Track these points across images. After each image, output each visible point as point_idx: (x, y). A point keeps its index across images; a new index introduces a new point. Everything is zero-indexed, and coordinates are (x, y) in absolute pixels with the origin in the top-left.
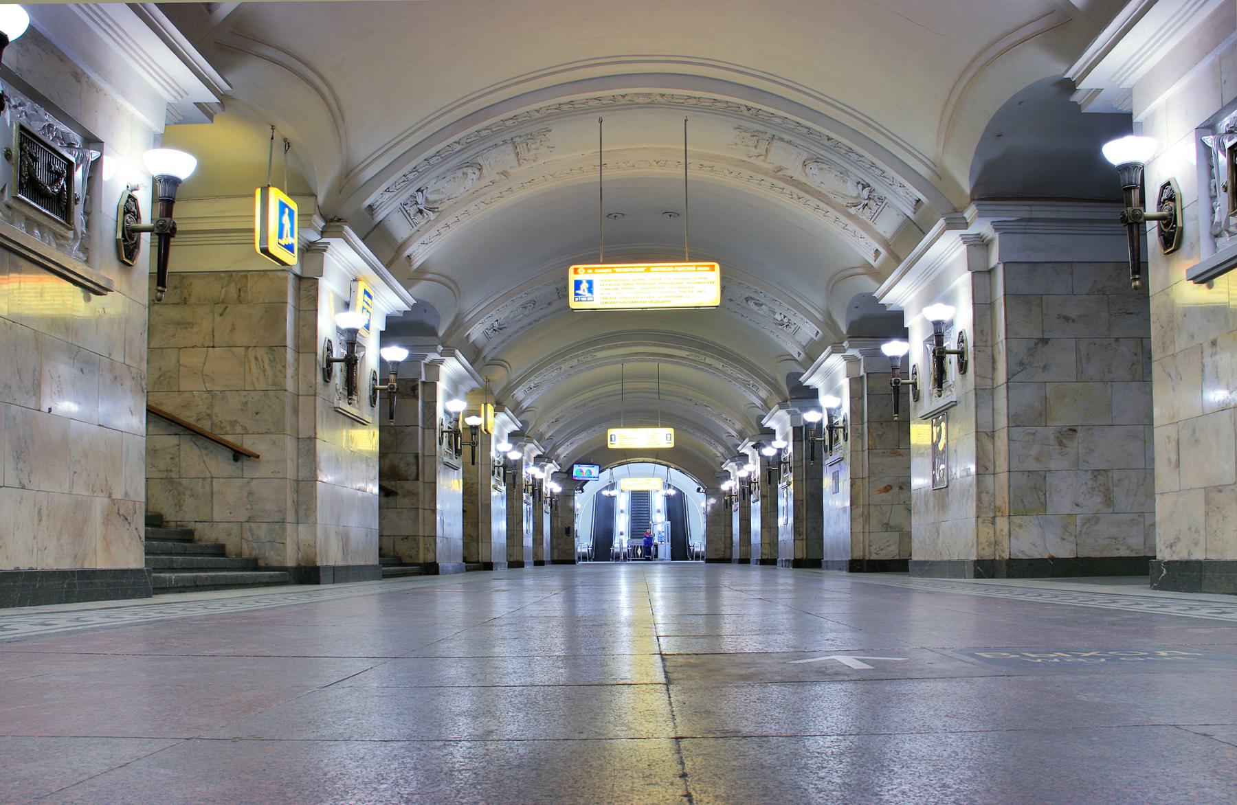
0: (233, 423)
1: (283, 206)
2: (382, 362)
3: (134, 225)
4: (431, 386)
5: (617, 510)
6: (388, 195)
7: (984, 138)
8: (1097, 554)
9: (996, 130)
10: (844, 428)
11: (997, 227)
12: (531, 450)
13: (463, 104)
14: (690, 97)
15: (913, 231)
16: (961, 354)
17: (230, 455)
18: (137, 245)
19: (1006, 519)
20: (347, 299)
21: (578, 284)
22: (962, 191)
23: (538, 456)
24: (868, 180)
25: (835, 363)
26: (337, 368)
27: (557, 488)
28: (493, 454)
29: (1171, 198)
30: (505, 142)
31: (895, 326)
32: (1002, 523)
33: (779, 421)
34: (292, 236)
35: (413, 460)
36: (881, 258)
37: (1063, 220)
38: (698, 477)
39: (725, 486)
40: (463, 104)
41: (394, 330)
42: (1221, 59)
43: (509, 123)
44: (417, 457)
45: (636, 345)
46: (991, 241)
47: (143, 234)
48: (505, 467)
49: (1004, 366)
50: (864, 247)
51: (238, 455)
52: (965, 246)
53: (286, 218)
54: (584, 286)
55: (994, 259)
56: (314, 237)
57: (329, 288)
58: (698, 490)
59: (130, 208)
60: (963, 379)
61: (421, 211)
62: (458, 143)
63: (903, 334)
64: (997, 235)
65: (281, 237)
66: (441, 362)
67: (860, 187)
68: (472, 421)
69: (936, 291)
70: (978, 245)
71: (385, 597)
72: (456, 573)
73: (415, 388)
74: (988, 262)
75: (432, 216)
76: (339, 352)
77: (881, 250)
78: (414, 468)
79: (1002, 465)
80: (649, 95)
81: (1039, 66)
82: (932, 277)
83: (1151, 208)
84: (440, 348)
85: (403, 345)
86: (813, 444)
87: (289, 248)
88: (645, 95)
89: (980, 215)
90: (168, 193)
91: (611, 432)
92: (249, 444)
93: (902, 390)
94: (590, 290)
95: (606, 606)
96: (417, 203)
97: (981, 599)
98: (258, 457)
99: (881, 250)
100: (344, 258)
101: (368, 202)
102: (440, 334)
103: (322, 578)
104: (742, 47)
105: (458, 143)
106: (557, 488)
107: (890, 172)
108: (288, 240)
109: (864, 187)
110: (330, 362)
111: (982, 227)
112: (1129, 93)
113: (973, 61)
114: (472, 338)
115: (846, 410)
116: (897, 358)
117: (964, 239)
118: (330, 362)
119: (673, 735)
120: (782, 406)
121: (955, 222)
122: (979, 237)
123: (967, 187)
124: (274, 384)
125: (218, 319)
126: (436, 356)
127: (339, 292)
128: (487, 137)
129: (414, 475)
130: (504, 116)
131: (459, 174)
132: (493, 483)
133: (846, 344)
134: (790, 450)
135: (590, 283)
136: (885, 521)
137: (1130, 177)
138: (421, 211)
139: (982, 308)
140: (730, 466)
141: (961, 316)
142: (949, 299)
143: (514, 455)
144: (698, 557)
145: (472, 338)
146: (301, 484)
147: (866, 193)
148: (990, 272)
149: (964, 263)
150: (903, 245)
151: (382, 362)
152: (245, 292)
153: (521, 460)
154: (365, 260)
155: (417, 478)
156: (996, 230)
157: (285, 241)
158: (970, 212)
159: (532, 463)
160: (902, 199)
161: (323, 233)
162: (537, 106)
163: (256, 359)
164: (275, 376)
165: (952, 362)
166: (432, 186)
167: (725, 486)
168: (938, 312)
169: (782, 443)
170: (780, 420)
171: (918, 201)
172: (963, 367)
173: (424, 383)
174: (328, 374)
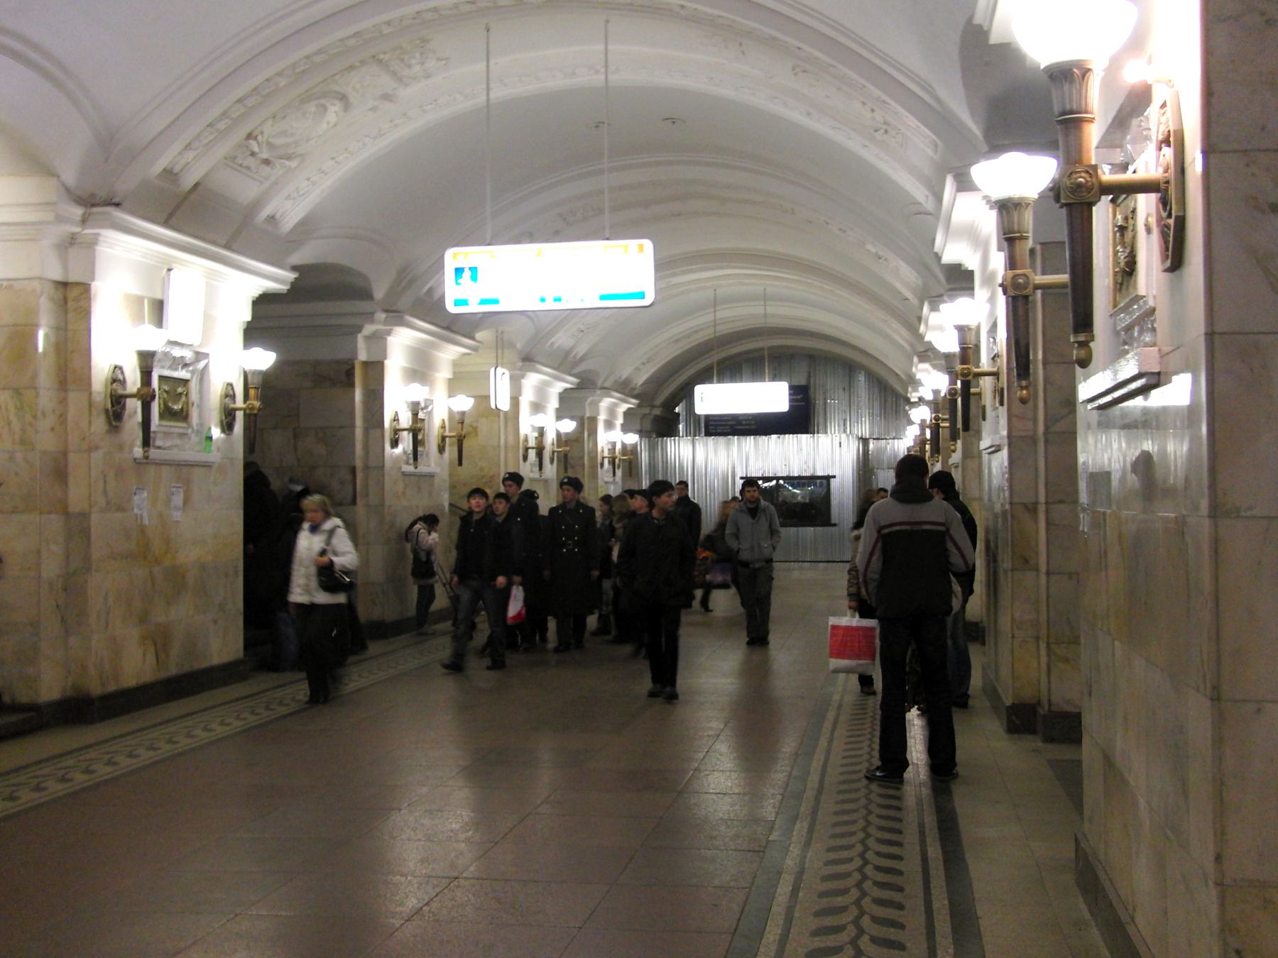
3: (232, 406)
4: (375, 369)
8: (241, 512)
18: (234, 418)
20: (159, 296)
26: (134, 406)
29: (1158, 428)
30: (363, 63)
35: (349, 477)
37: (237, 700)
38: (897, 484)
42: (1168, 467)
43: (351, 42)
44: (353, 470)
45: (722, 268)
47: (128, 400)
59: (229, 394)
60: (1148, 239)
61: (267, 162)
66: (389, 333)
71: (895, 457)
72: (66, 485)
73: (350, 373)
76: (532, 443)
78: (349, 488)
82: (703, 425)
83: (387, 424)
84: (381, 316)
85: (267, 346)
90: (460, 419)
91: (454, 257)
94: (474, 278)
95: (993, 39)
96: (253, 154)
97: (1086, 112)
100: (125, 261)
101: (158, 167)
102: (379, 293)
103: (342, 355)
104: (548, 63)
110: (527, 449)
116: (1085, 380)
118: (527, 449)
119: (58, 277)
124: (23, 442)
127: (136, 291)
128: (219, 119)
130: (240, 92)
131: (312, 108)
144: (349, 598)
146: (1217, 337)
153: (190, 426)
154: (351, 314)
155: (354, 502)
161: (84, 221)
164: (23, 430)
166: (268, 128)
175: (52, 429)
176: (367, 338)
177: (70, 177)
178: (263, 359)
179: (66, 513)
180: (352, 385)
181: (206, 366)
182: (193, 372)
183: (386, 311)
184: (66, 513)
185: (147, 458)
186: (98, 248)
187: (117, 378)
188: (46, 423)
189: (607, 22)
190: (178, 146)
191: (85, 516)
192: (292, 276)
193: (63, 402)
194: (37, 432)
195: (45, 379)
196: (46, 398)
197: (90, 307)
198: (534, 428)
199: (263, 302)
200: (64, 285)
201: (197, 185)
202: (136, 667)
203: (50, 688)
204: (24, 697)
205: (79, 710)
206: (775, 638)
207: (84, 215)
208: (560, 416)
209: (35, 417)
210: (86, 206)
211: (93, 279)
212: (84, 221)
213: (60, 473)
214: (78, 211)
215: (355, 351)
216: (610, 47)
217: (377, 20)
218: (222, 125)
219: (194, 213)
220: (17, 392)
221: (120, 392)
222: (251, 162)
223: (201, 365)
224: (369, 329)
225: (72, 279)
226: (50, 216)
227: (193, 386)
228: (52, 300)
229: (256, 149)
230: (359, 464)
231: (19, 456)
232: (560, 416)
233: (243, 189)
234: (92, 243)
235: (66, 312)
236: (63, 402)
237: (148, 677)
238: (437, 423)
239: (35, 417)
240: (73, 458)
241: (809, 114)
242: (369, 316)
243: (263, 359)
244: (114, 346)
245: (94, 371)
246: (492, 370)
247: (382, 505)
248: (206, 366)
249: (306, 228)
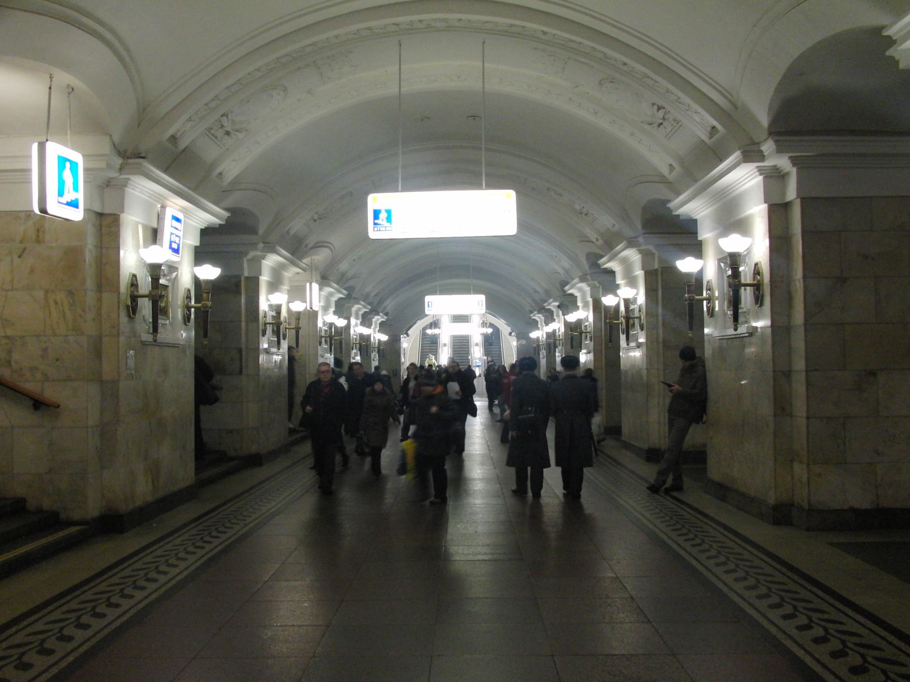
0: (33, 369)
1: (62, 161)
2: (197, 282)
5: (802, 658)
6: (190, 124)
7: (785, 77)
9: (794, 72)
10: (709, 300)
11: (794, 161)
12: (359, 309)
13: (666, 53)
14: (572, 41)
15: (709, 155)
16: (757, 287)
17: (31, 403)
19: (804, 466)
20: (155, 226)
21: (376, 214)
22: (756, 122)
23: (365, 316)
24: (664, 105)
25: (744, 179)
27: (384, 338)
28: (320, 324)
29: (759, 273)
30: (308, 65)
31: (685, 236)
32: (799, 469)
33: (580, 290)
34: (76, 189)
36: (674, 173)
39: (534, 335)
40: (666, 53)
41: (209, 246)
44: (240, 351)
46: (788, 174)
48: (331, 337)
49: (802, 305)
50: (659, 157)
51: (38, 404)
52: (761, 178)
53: (67, 174)
54: (383, 215)
55: (791, 193)
56: (114, 174)
57: (132, 225)
58: (510, 334)
61: (228, 133)
62: (258, 70)
63: (696, 249)
64: (794, 171)
65: (61, 194)
66: (263, 258)
67: (655, 107)
68: (298, 306)
69: (732, 221)
70: (774, 178)
73: (238, 285)
74: (784, 193)
75: (240, 135)
77: (674, 164)
79: (800, 408)
80: (445, 20)
81: (871, 18)
84: (261, 245)
85: (215, 264)
86: (611, 327)
87: (74, 204)
88: (441, 20)
89: (780, 150)
91: (375, 201)
92: (50, 393)
93: (631, 322)
94: (389, 219)
96: (222, 126)
98: (59, 406)
99: (719, 126)
101: (171, 131)
102: (261, 231)
105: (190, 119)
106: (384, 338)
107: (686, 99)
108: (69, 196)
109: (659, 108)
110: (134, 298)
111: (783, 162)
112: (705, 445)
113: (841, 612)
114: (292, 232)
115: (641, 299)
117: (761, 171)
118: (134, 298)
119: (99, 210)
120: (583, 279)
121: (751, 154)
122: (775, 168)
123: (765, 121)
125: (17, 261)
126: (259, 253)
129: (395, 26)
132: (320, 352)
133: (588, 277)
134: (591, 319)
135: (389, 212)
136: (499, 418)
137: (503, 411)
138: (228, 133)
139: (779, 242)
140: (539, 317)
141: (755, 246)
142: (740, 226)
143: (341, 323)
145: (292, 232)
147: (661, 112)
148: (787, 206)
149: (760, 195)
150: (704, 159)
151: (197, 282)
152: (44, 232)
155: (241, 372)
156: (794, 165)
157: (67, 198)
158: (768, 147)
159: (333, 309)
160: (699, 123)
161: (121, 169)
162: (335, 32)
163: (56, 303)
165: (747, 296)
167: (534, 335)
168: (733, 243)
169: (583, 314)
170: (580, 290)
171: (714, 127)
172: (759, 299)
173: (247, 278)
174: (133, 309)
175: (94, 320)
176: (248, 260)
177: (117, 138)
178: (210, 272)
179: (102, 382)
180: (239, 293)
181: (177, 276)
182: (169, 280)
183: (264, 243)
184: (102, 382)
185: (155, 341)
186: (127, 189)
187: (134, 283)
188: (90, 316)
189: (484, 43)
190: (185, 117)
191: (115, 382)
192: (226, 214)
193: (100, 300)
194: (85, 321)
195: (90, 283)
196: (90, 297)
197: (119, 231)
198: (271, 306)
199: (206, 233)
200: (100, 215)
201: (184, 150)
202: (144, 491)
203: (93, 508)
204: (76, 516)
205: (111, 524)
206: (254, 449)
207: (121, 165)
208: (201, 255)
209: (84, 311)
210: (123, 158)
211: (123, 212)
212: (121, 169)
213: (97, 351)
214: (119, 161)
215: (242, 268)
216: (486, 65)
217: (416, 18)
218: (213, 105)
219: (185, 168)
220: (71, 293)
221: (136, 293)
222: (220, 133)
223: (174, 274)
224: (252, 254)
225: (107, 211)
226: (103, 165)
227: (170, 289)
228: (94, 225)
229: (225, 124)
230: (243, 347)
231: (72, 339)
232: (201, 255)
233: (209, 151)
234: (125, 184)
235: (101, 236)
236: (100, 300)
237: (150, 499)
238: (181, 294)
239: (84, 311)
240: (105, 340)
241: (596, 113)
242: (254, 246)
243: (210, 272)
244: (134, 257)
245: (121, 278)
246: (308, 284)
247: (258, 375)
248: (177, 276)
249: (235, 185)
